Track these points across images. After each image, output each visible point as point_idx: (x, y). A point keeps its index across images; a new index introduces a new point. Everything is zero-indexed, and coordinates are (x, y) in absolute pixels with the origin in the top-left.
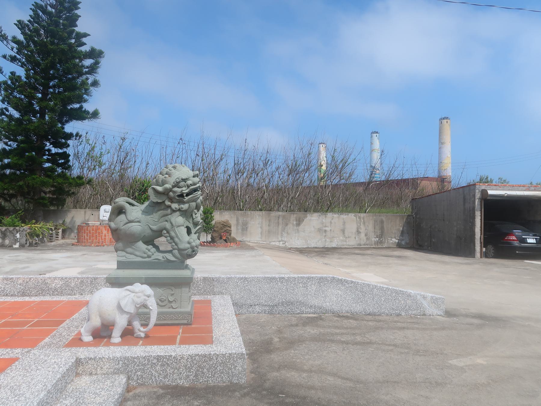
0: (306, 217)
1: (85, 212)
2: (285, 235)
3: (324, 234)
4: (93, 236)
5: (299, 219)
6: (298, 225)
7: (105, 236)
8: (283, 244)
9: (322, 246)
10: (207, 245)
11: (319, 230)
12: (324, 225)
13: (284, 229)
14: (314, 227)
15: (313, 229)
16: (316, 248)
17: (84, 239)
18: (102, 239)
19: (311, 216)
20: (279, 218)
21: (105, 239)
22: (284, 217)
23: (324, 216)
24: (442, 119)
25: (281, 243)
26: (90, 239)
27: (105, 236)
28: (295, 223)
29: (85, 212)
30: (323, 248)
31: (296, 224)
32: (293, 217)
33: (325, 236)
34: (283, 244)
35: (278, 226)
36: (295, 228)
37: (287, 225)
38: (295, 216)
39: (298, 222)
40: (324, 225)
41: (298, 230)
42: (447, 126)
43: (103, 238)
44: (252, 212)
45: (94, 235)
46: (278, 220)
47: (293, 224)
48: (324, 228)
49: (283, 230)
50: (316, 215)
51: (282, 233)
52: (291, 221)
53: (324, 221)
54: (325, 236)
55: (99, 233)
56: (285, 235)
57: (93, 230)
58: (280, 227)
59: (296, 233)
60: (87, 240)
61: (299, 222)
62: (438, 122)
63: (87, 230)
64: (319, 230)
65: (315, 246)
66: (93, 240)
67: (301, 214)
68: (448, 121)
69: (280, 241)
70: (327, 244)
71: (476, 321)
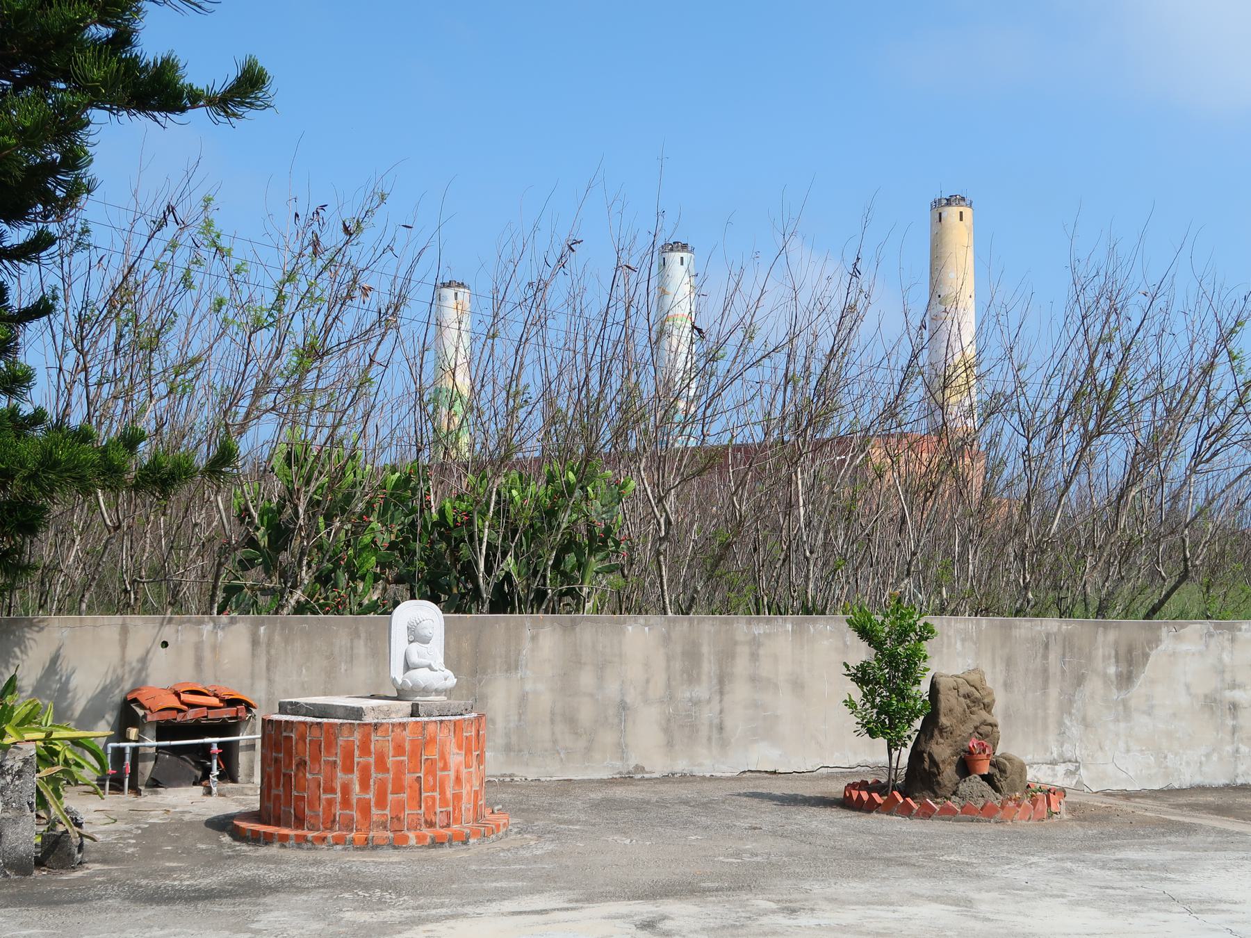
0: (1157, 641)
1: (124, 630)
2: (1075, 730)
3: (1230, 722)
4: (399, 789)
5: (1130, 651)
6: (1126, 679)
7: (458, 779)
8: (1069, 773)
9: (1222, 781)
10: (888, 808)
11: (1211, 703)
12: (1228, 677)
13: (1071, 702)
14: (1188, 687)
15: (1184, 700)
16: (1202, 789)
17: (346, 803)
18: (444, 802)
19: (1177, 638)
20: (1046, 646)
21: (457, 797)
22: (1068, 643)
23: (1227, 635)
24: (937, 204)
25: (1061, 769)
26: (381, 803)
27: (458, 779)
28: (1112, 670)
29: (124, 630)
30: (1227, 786)
31: (1119, 676)
32: (1105, 640)
33: (1234, 730)
34: (1069, 773)
35: (1045, 687)
36: (1114, 695)
37: (1080, 680)
38: (1112, 635)
39: (1123, 668)
40: (1228, 677)
41: (1125, 703)
42: (961, 231)
43: (449, 793)
44: (743, 627)
45: (408, 778)
46: (1045, 657)
47: (1105, 676)
48: (1230, 695)
49: (1066, 706)
50: (1195, 629)
51: (1061, 724)
52: (1099, 664)
53: (1226, 658)
54: (1234, 730)
55: (431, 771)
56: (1075, 730)
57: (399, 750)
58: (1054, 691)
59: (1117, 720)
60: (365, 809)
61: (1130, 664)
62: (927, 215)
63: (365, 749)
64: (1211, 703)
65: (1198, 780)
66: (400, 806)
67: (1134, 628)
68: (967, 212)
69: (1053, 763)
70: (1241, 768)
71: (56, 898)
